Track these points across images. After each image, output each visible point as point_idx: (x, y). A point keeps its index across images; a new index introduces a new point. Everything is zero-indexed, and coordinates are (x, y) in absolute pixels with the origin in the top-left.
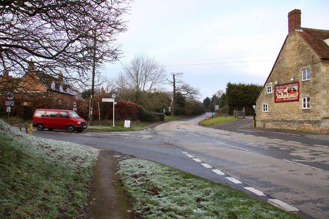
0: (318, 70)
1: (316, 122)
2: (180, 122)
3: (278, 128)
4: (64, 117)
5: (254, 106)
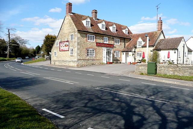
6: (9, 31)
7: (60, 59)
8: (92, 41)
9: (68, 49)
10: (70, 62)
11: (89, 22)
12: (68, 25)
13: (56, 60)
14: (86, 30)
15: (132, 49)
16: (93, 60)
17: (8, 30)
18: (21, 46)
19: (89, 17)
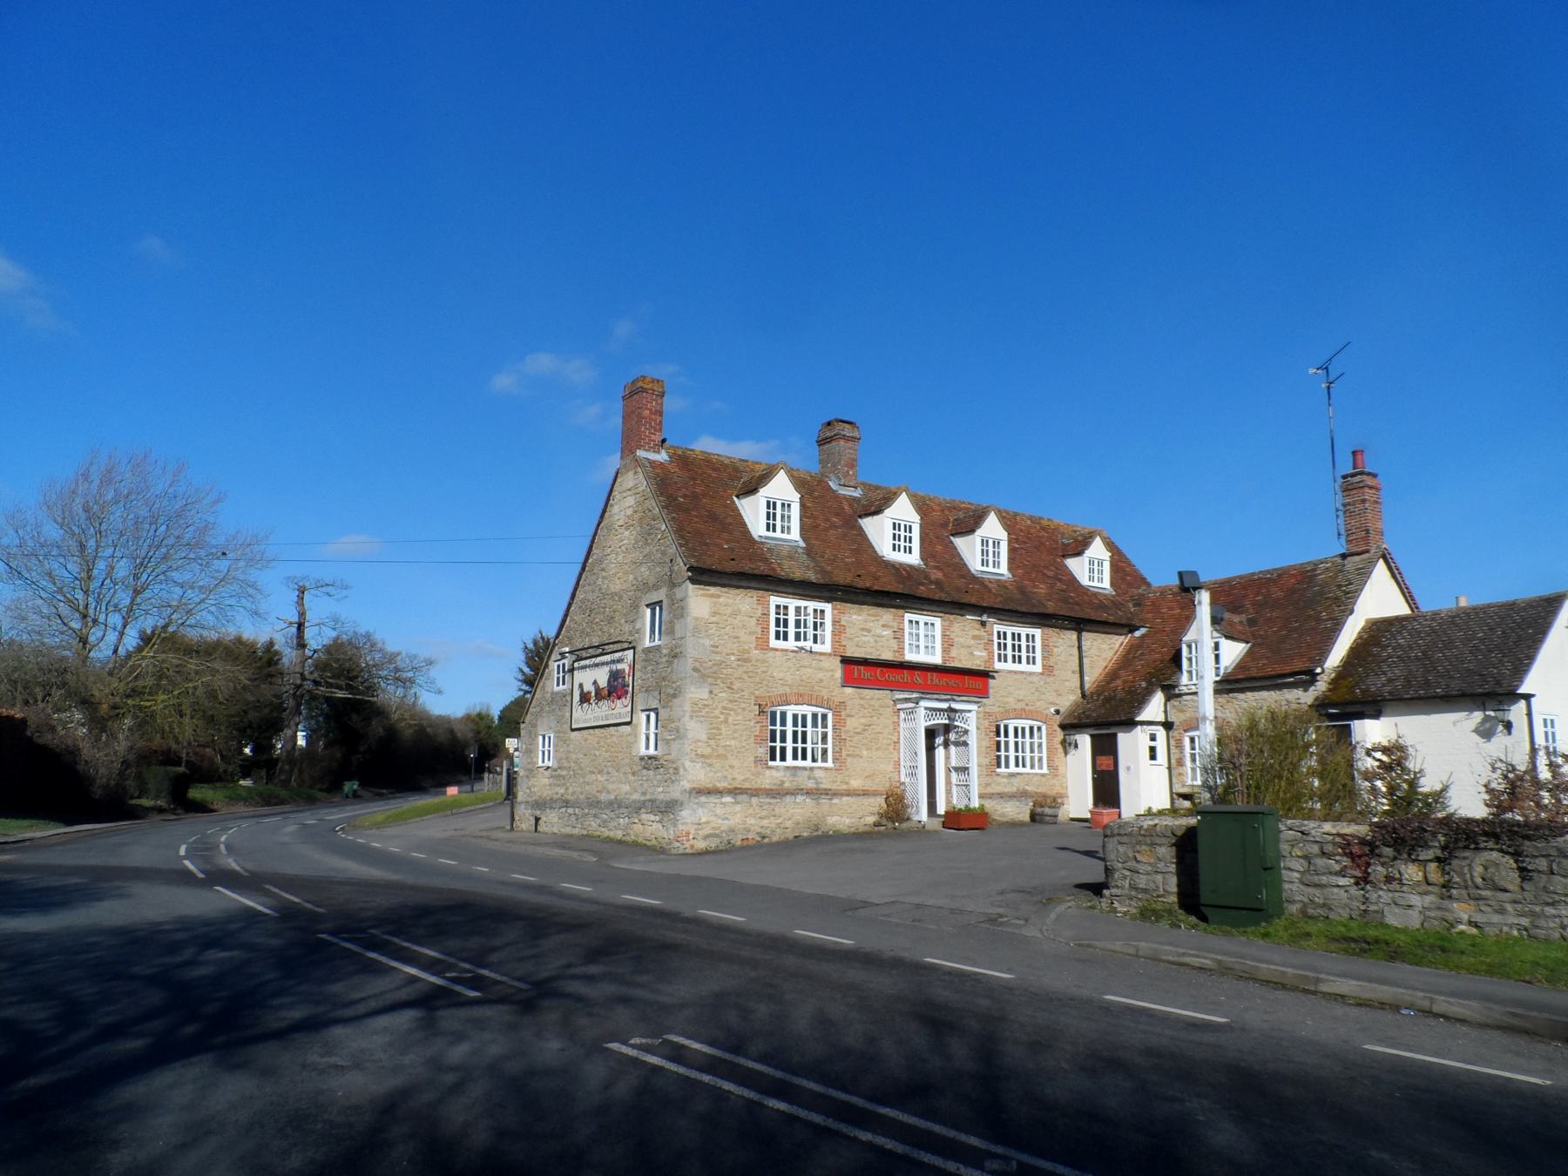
0: (679, 609)
1: (667, 809)
2: (952, 665)
3: (576, 831)
4: (1064, 824)
5: (511, 743)
6: (301, 599)
7: (573, 790)
8: (1024, 667)
9: (629, 720)
10: (637, 808)
11: (786, 506)
12: (628, 537)
13: (547, 793)
14: (762, 568)
15: (1141, 700)
16: (816, 793)
17: (294, 596)
18: (389, 695)
19: (785, 464)
